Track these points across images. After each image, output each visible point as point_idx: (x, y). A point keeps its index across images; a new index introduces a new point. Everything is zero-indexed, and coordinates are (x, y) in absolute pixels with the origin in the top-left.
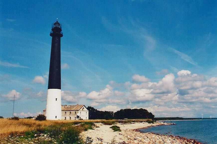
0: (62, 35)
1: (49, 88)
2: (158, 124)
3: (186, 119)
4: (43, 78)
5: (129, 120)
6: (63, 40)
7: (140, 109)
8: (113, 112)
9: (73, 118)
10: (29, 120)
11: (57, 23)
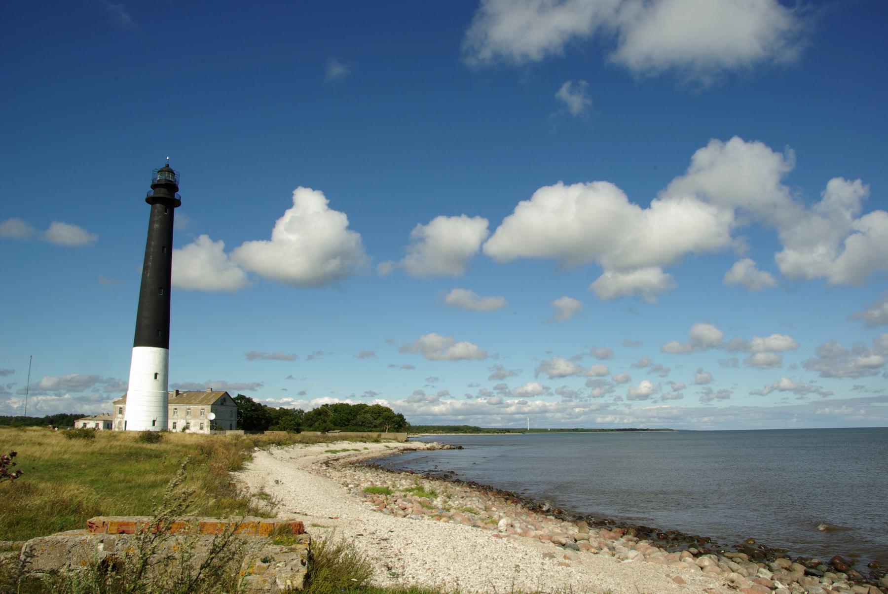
0: (178, 203)
1: (137, 344)
2: (593, 579)
3: (488, 431)
4: (128, 319)
5: (343, 434)
6: (180, 219)
7: (282, 214)
8: (301, 412)
9: (195, 425)
10: (17, 435)
11: (168, 170)
